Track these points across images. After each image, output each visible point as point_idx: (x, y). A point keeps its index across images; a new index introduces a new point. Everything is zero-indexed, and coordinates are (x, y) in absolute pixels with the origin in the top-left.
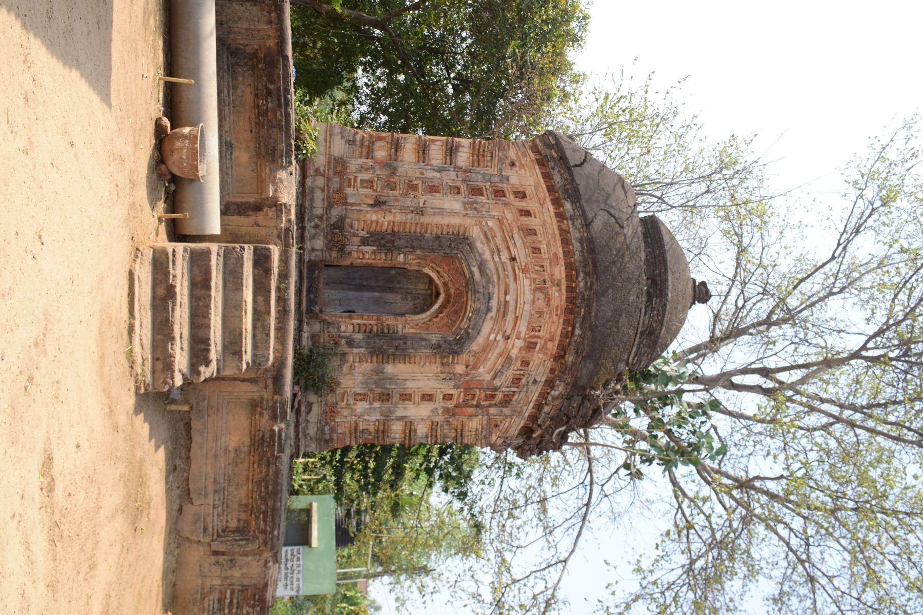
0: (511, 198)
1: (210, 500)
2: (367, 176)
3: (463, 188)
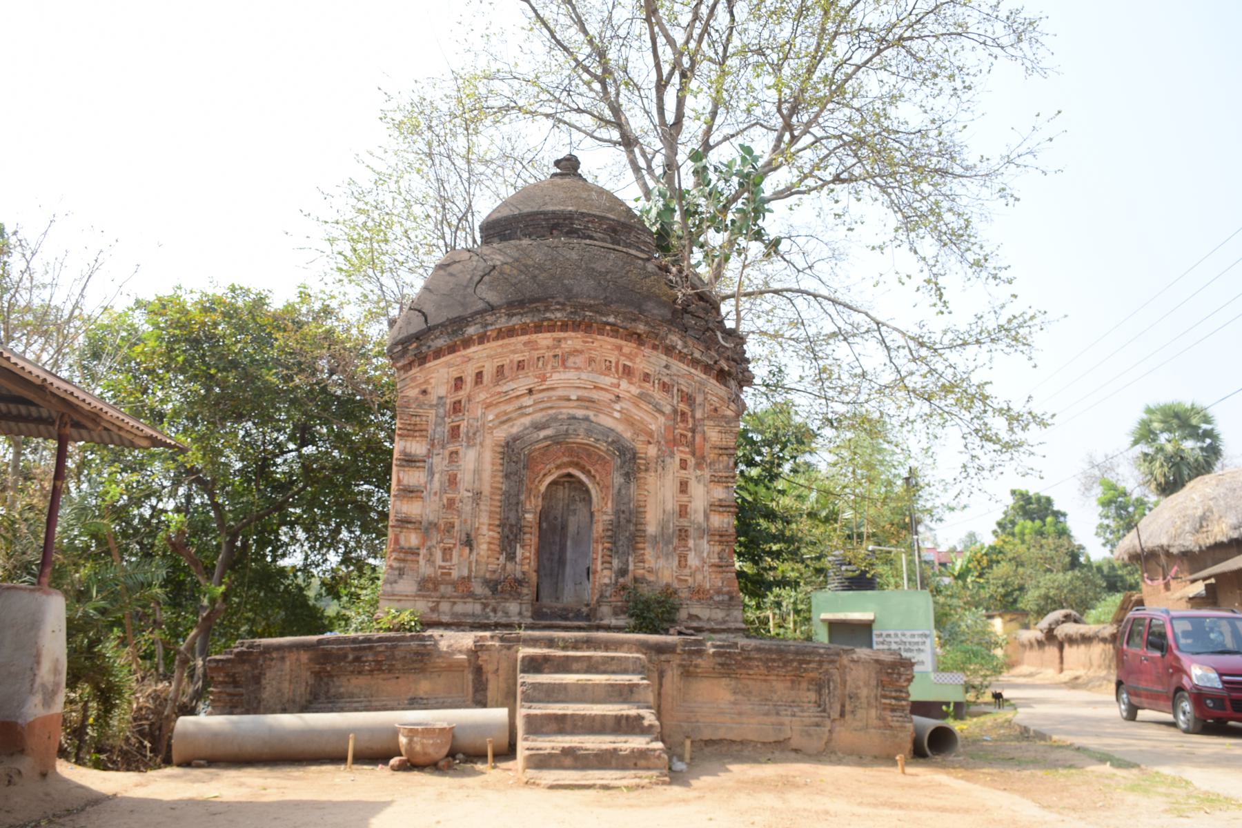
0: (462, 394)
1: (787, 720)
2: (438, 555)
3: (451, 448)
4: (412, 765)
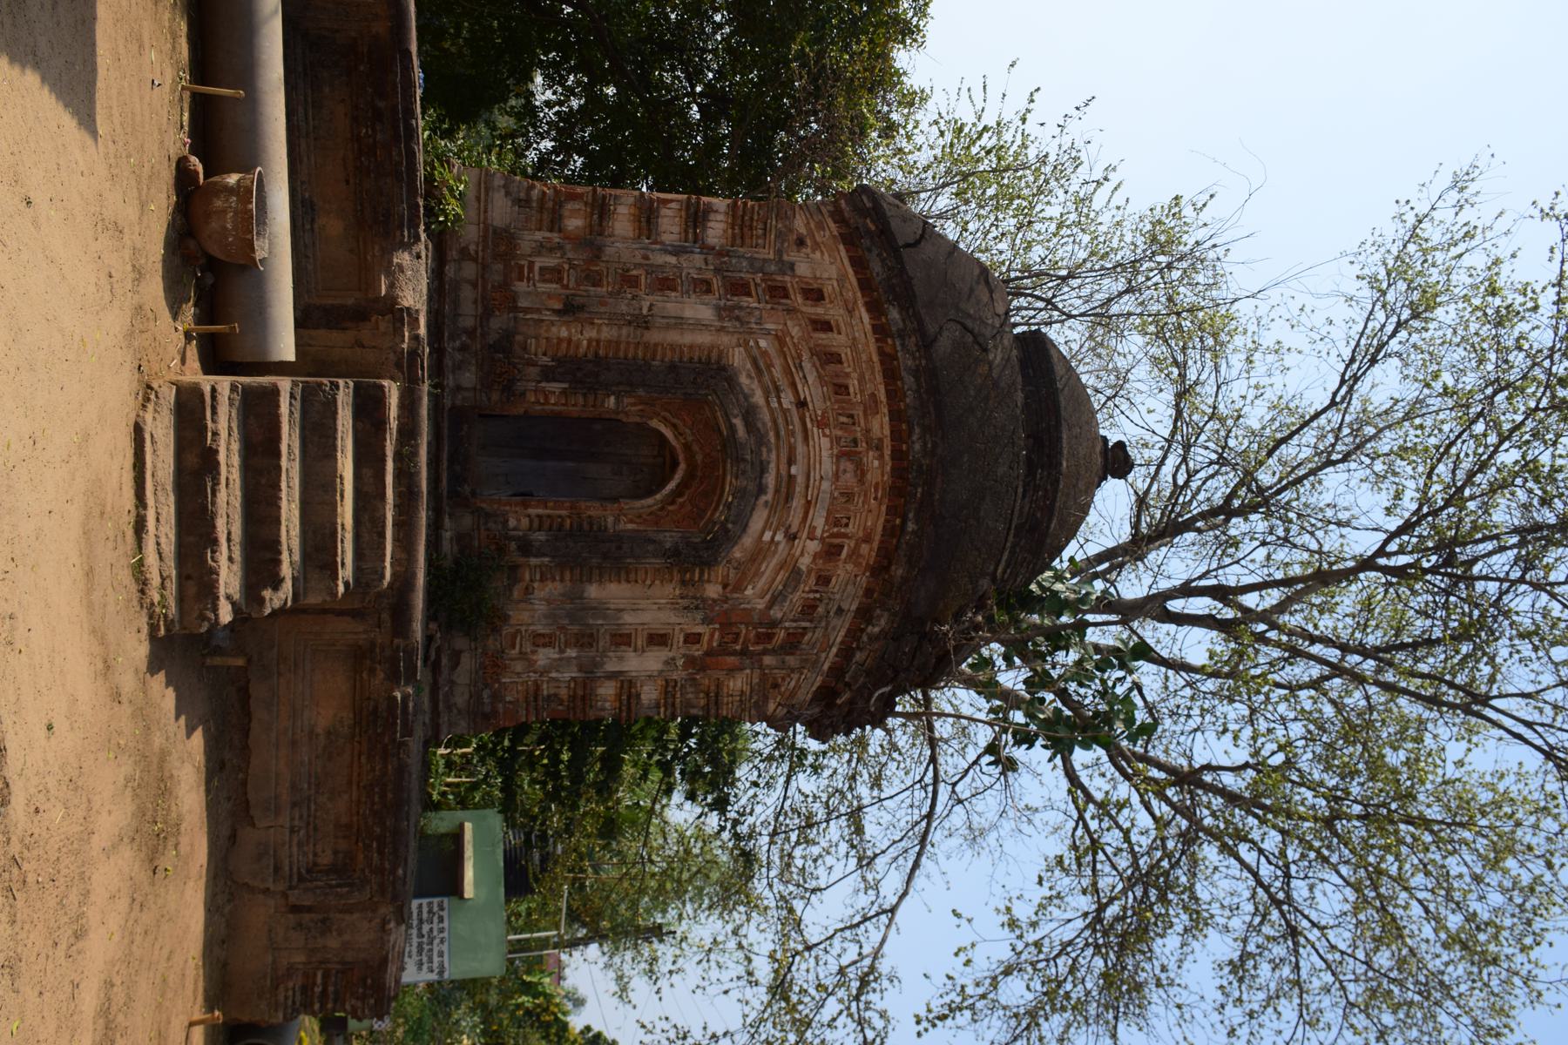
1: (284, 820)
2: (550, 261)
3: (716, 283)
4: (190, 198)
